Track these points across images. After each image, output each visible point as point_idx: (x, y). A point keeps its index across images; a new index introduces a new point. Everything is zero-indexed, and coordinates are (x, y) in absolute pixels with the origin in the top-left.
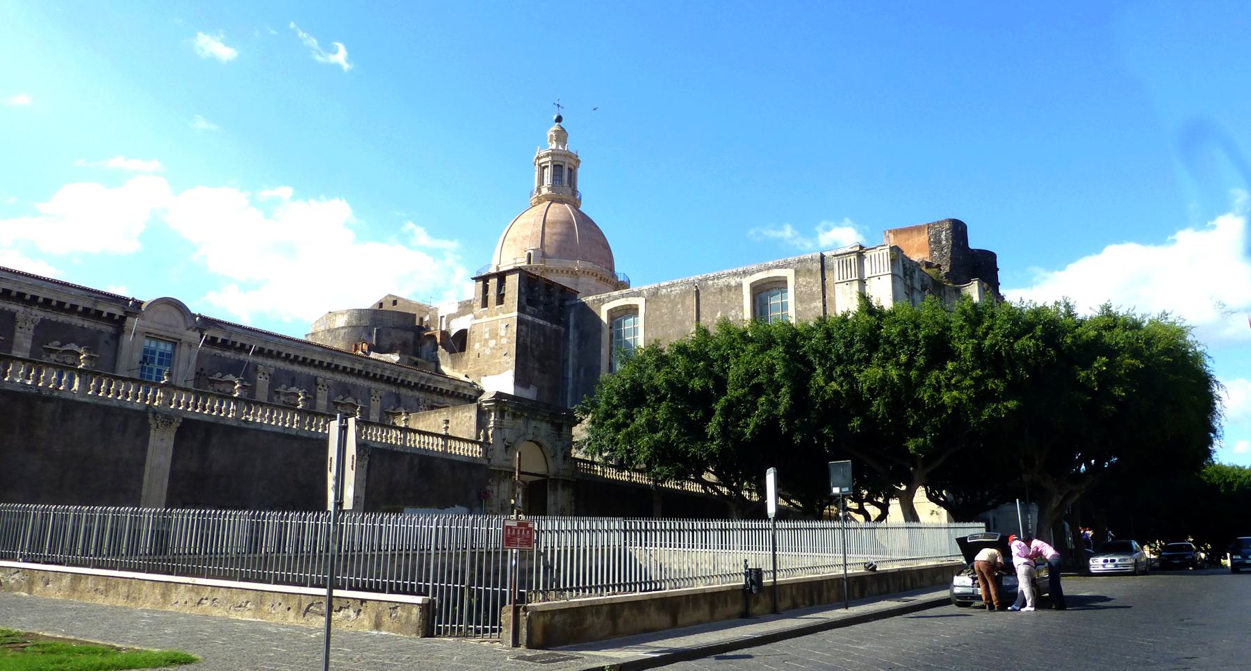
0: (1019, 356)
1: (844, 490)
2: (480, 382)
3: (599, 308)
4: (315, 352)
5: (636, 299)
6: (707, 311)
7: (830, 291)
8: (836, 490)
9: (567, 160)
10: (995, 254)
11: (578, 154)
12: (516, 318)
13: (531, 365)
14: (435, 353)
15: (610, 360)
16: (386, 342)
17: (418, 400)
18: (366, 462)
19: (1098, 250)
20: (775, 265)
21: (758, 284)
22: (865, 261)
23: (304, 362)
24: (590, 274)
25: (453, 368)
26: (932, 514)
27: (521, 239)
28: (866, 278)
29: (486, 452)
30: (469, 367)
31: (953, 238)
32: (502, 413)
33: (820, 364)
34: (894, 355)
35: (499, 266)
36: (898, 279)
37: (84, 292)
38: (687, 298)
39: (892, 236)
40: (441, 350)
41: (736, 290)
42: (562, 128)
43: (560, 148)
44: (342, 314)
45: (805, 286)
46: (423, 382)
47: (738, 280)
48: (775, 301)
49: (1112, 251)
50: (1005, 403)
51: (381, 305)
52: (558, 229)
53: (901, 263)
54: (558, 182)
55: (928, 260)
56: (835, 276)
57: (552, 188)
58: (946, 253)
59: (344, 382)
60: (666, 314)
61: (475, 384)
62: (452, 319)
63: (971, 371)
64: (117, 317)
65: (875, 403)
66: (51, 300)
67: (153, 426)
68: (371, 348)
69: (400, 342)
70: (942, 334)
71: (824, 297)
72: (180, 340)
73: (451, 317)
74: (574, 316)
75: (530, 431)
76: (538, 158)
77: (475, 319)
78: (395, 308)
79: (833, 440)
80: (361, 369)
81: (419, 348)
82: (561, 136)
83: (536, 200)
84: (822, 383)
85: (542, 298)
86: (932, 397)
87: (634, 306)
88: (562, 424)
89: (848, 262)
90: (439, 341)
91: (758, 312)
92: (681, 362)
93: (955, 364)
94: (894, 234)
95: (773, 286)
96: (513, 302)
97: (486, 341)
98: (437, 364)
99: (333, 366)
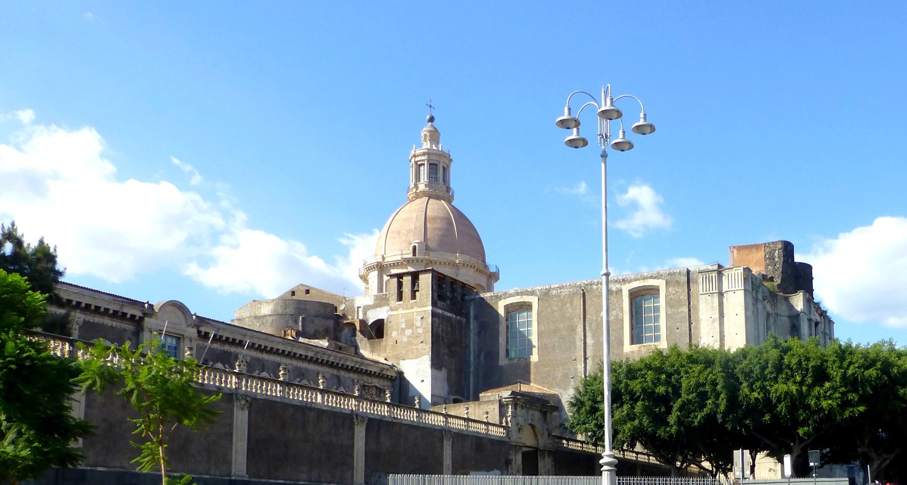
0: (867, 380)
1: (815, 464)
2: (398, 364)
3: (497, 304)
4: (279, 343)
5: (530, 297)
6: (592, 310)
7: (694, 299)
8: (812, 464)
9: (442, 160)
10: (811, 266)
11: (451, 154)
12: (430, 312)
13: (443, 351)
14: (353, 338)
15: (507, 347)
16: (311, 329)
17: (353, 380)
18: (451, 442)
19: (870, 223)
20: (649, 276)
21: (635, 290)
22: (724, 278)
23: (271, 351)
24: (469, 266)
25: (372, 352)
26: (770, 471)
27: (405, 232)
28: (724, 291)
29: (508, 434)
30: (387, 351)
31: (784, 256)
32: (515, 406)
33: (745, 380)
34: (792, 376)
35: (385, 256)
36: (749, 293)
37: (110, 297)
38: (575, 298)
39: (735, 251)
40: (359, 337)
41: (616, 294)
42: (435, 128)
43: (434, 148)
44: (268, 303)
45: (674, 294)
46: (357, 366)
47: (618, 286)
48: (648, 304)
49: (883, 223)
50: (858, 408)
51: (293, 293)
52: (438, 225)
53: (750, 279)
54: (433, 179)
55: (764, 273)
56: (700, 287)
57: (429, 185)
58: (778, 268)
59: (299, 367)
60: (557, 311)
61: (394, 366)
62: (369, 310)
63: (839, 388)
64: (137, 318)
65: (780, 406)
66: (91, 305)
67: (356, 423)
68: (299, 334)
69: (323, 329)
70: (822, 364)
71: (689, 304)
72: (183, 335)
73: (366, 309)
74: (474, 308)
75: (530, 418)
76: (415, 156)
77: (392, 311)
78: (307, 298)
79: (752, 428)
80: (290, 351)
81: (339, 334)
82: (434, 136)
83: (414, 195)
84: (748, 393)
85: (448, 294)
86: (815, 403)
87: (528, 304)
88: (547, 412)
89: (710, 279)
90: (358, 328)
91: (634, 313)
92: (650, 375)
93: (830, 383)
94: (737, 250)
95: (648, 293)
96: (427, 298)
97: (403, 330)
98: (357, 348)
99: (292, 354)
